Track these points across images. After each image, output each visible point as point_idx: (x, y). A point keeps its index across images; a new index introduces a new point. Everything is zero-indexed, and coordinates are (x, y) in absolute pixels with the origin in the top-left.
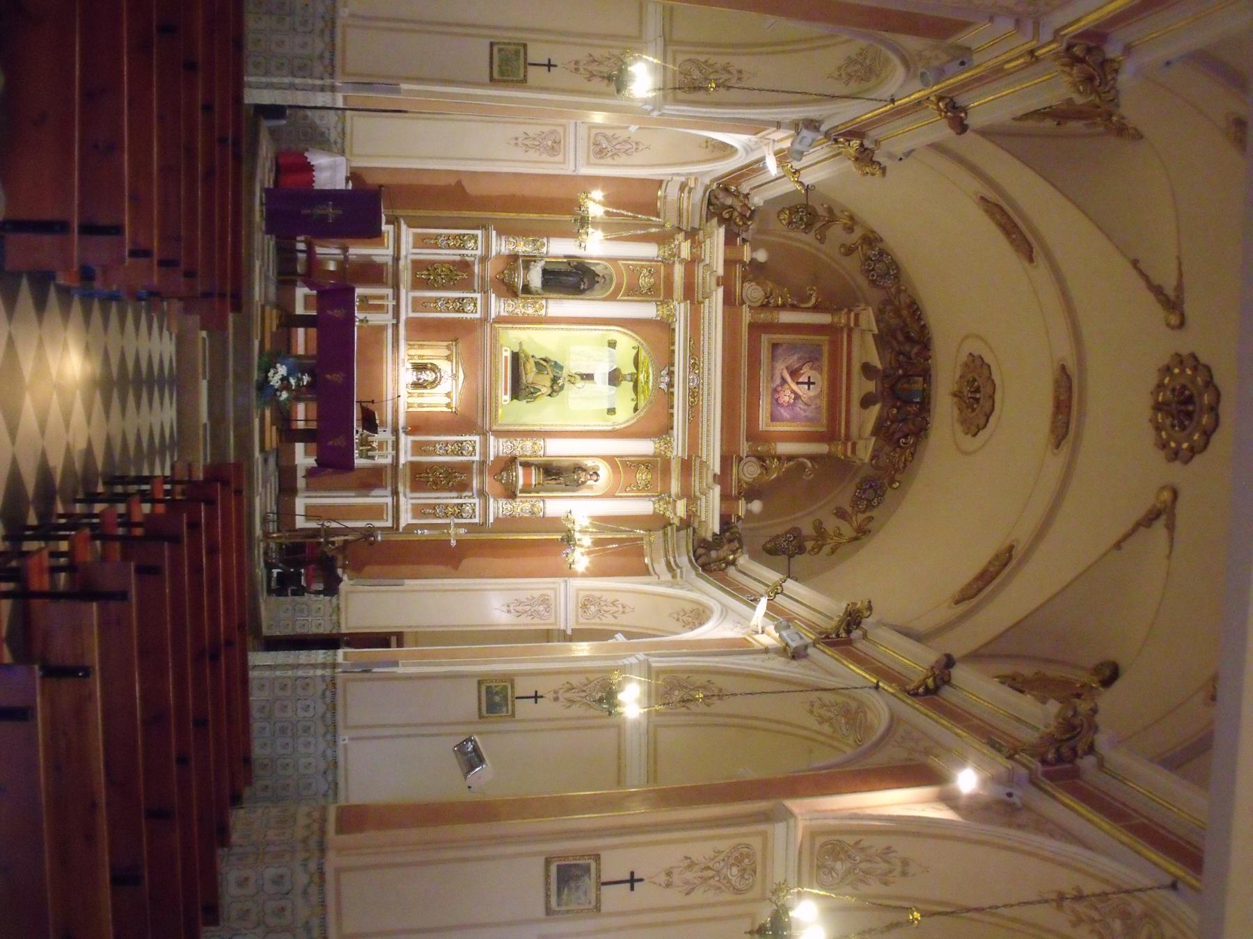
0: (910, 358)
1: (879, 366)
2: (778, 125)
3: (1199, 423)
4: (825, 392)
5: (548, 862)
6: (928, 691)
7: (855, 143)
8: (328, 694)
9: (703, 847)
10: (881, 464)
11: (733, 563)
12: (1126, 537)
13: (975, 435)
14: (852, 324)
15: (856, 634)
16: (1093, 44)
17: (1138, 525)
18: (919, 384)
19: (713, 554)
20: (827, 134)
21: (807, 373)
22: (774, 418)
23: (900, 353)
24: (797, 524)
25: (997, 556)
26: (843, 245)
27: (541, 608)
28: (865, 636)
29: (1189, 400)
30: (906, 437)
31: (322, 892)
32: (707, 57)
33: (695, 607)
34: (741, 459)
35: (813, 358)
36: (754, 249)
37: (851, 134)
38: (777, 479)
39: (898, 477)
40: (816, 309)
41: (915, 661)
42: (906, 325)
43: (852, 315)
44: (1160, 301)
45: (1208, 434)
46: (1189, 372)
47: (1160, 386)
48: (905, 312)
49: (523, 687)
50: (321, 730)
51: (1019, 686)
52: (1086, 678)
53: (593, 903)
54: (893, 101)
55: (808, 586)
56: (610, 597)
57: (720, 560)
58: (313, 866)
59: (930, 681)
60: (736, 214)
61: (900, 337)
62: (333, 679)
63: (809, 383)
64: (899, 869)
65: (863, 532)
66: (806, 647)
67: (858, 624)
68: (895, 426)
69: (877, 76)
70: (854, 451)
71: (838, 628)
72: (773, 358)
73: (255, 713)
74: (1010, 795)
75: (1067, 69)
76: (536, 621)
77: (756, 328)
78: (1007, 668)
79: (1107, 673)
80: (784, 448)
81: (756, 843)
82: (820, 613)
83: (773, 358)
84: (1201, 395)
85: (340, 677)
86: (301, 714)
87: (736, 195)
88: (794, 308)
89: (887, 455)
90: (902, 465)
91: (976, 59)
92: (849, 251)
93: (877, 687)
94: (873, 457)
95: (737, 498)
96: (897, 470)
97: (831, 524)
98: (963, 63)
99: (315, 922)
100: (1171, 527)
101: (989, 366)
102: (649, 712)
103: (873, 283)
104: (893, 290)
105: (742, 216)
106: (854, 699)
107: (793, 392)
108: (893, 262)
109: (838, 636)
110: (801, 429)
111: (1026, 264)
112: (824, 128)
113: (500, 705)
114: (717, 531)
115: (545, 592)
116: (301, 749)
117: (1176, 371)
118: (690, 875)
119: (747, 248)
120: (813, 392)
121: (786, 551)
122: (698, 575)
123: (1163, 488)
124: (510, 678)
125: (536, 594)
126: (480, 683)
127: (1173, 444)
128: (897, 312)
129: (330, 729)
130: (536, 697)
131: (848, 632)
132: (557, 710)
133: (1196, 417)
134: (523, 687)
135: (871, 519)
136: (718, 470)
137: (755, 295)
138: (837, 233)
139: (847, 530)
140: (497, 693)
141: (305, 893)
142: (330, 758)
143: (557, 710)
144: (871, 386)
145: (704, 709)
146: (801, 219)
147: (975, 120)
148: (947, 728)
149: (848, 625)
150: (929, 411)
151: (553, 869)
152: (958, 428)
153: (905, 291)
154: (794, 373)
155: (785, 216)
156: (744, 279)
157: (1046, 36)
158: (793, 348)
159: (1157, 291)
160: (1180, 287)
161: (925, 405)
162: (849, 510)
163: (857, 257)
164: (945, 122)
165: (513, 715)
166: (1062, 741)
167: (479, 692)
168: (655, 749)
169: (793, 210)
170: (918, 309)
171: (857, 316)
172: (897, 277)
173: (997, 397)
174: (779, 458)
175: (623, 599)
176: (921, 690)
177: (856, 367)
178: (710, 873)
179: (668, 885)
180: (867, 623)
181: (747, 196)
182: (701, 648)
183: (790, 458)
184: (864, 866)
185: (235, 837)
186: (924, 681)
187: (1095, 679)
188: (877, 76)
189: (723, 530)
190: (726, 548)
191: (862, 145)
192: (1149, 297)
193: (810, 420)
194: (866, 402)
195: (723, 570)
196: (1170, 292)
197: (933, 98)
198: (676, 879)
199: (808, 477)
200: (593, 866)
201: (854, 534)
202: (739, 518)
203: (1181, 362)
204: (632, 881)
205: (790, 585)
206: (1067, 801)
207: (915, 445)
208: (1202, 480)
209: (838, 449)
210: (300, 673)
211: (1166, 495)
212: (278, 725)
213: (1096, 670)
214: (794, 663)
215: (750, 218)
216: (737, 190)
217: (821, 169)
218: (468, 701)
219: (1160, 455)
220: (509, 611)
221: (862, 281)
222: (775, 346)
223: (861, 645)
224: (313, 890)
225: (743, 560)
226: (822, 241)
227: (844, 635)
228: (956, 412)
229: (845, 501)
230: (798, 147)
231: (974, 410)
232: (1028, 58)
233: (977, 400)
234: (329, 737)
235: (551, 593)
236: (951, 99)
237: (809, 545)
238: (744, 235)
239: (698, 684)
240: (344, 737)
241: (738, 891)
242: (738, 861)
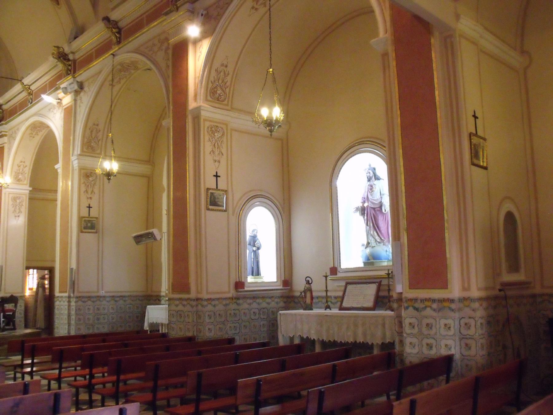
5: (208, 209)
8: (83, 300)
9: (207, 146)
15: (71, 57)
27: (18, 201)
28: (73, 53)
31: (214, 300)
33: (30, 128)
41: (96, 34)
49: (85, 213)
50: (98, 303)
53: (223, 192)
56: (16, 168)
58: (205, 303)
62: (77, 297)
64: (224, 68)
67: (66, 55)
71: (64, 64)
73: (91, 332)
74: (202, 15)
76: (24, 204)
81: (207, 124)
82: (50, 70)
85: (76, 294)
86: (91, 312)
99: (224, 302)
102: (115, 157)
109: (70, 65)
113: (92, 224)
115: (10, 199)
116: (106, 311)
118: (217, 153)
122: (6, 124)
124: (80, 218)
125: (11, 203)
126: (82, 232)
129: (446, 304)
130: (89, 207)
131: (69, 60)
132: (95, 197)
134: (85, 213)
140: (87, 224)
141: (214, 306)
142: (461, 305)
143: (95, 197)
145: (101, 133)
148: (148, 30)
149: (65, 59)
151: (211, 207)
165: (97, 218)
167: (86, 232)
168: (139, 160)
175: (17, 162)
178: (216, 144)
179: (219, 162)
180: (67, 50)
184: (220, 82)
185: (190, 334)
195: (3, 111)
198: (217, 159)
200: (211, 191)
204: (217, 176)
205: (26, 81)
210: (73, 312)
212: (96, 322)
214: (86, 89)
218: (89, 237)
220: (19, 216)
224: (213, 303)
227: (70, 63)
234: (101, 299)
235: (11, 196)
240: (102, 293)
241: (223, 135)
242: (213, 132)
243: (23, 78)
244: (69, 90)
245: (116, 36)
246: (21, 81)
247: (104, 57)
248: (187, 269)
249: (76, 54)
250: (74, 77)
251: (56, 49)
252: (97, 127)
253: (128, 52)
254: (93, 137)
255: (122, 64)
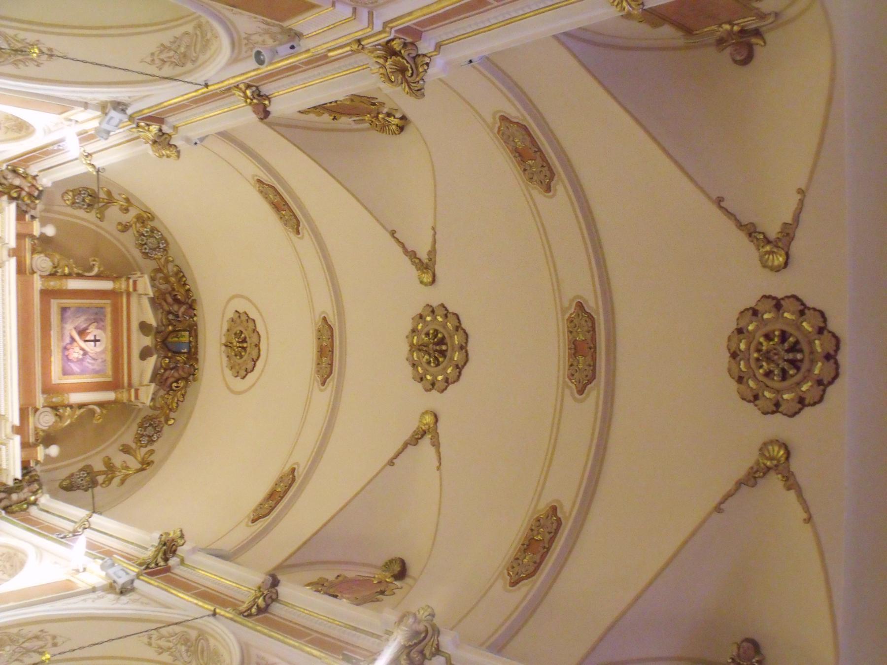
0: (177, 316)
1: (154, 324)
2: (86, 105)
3: (452, 359)
4: (110, 347)
6: (260, 611)
7: (154, 128)
10: (158, 405)
11: (35, 503)
12: (397, 456)
13: (244, 378)
14: (131, 289)
15: (173, 561)
16: (409, 40)
17: (406, 445)
18: (185, 337)
19: (14, 497)
20: (131, 118)
21: (93, 332)
22: (65, 372)
23: (169, 312)
24: (89, 462)
25: (281, 479)
26: (120, 224)
28: (182, 562)
29: (442, 341)
30: (177, 381)
32: (16, 32)
34: (36, 410)
35: (97, 318)
36: (43, 224)
37: (157, 119)
38: (70, 425)
39: (172, 415)
40: (98, 277)
41: (242, 580)
42: (174, 289)
43: (131, 281)
44: (413, 263)
45: (459, 368)
46: (439, 319)
47: (414, 331)
48: (173, 279)
51: (331, 591)
52: (379, 574)
54: (207, 85)
55: (113, 518)
57: (20, 502)
59: (260, 601)
60: (24, 193)
61: (170, 300)
63: (96, 341)
65: (146, 464)
66: (132, 581)
67: (174, 552)
68: (167, 373)
69: (194, 61)
70: (137, 397)
71: (155, 557)
72: (63, 319)
75: (381, 61)
77: (47, 294)
78: (314, 575)
79: (397, 568)
80: (76, 398)
83: (63, 319)
84: (452, 337)
87: (25, 177)
88: (80, 276)
89: (162, 397)
90: (175, 405)
91: (305, 44)
92: (125, 228)
93: (214, 614)
94: (153, 399)
95: (35, 445)
96: (171, 410)
97: (119, 459)
98: (292, 47)
100: (436, 444)
101: (254, 321)
103: (146, 255)
104: (163, 260)
105: (30, 195)
106: (193, 628)
107: (82, 349)
108: (163, 238)
109: (157, 564)
110: (89, 380)
111: (293, 236)
112: (130, 111)
114: (19, 476)
117: (429, 319)
119: (36, 224)
120: (100, 347)
121: (80, 485)
123: (426, 412)
127: (429, 377)
128: (166, 279)
131: (166, 560)
133: (448, 354)
135: (152, 452)
136: (17, 422)
137: (44, 266)
138: (114, 213)
139: (134, 464)
144: (148, 341)
146: (84, 200)
147: (277, 108)
149: (165, 553)
150: (197, 360)
152: (228, 373)
153: (172, 261)
154: (82, 333)
155: (69, 196)
156: (34, 251)
157: (378, 27)
158: (80, 310)
159: (412, 255)
160: (433, 252)
161: (193, 355)
162: (133, 446)
163: (131, 233)
164: (249, 109)
166: (410, 646)
169: (77, 192)
170: (184, 276)
171: (135, 282)
172: (165, 250)
173: (263, 346)
174: (71, 406)
176: (254, 610)
177: (135, 326)
180: (181, 551)
181: (34, 177)
182: (27, 598)
183: (81, 406)
186: (254, 602)
187: (388, 574)
188: (194, 61)
189: (24, 475)
190: (26, 490)
191: (160, 130)
192: (406, 260)
193: (96, 372)
194: (145, 354)
196: (423, 255)
197: (242, 86)
199: (97, 421)
201: (139, 466)
202: (37, 462)
203: (433, 312)
206: (292, 642)
207: (185, 387)
208: (824, 435)
209: (124, 396)
211: (429, 419)
213: (388, 565)
214: (124, 599)
215: (38, 198)
216: (24, 173)
217: (116, 154)
219: (419, 386)
221: (137, 254)
222: (64, 310)
223: (180, 571)
225: (44, 499)
226: (101, 219)
227: (162, 563)
228: (225, 359)
229: (128, 438)
230: (105, 126)
231: (241, 357)
232: (355, 47)
233: (244, 349)
236: (257, 88)
237: (100, 479)
238: (33, 212)
239: (30, 635)
243: (101, 514)
244: (111, 571)
245: (252, 607)
246: (94, 512)
247: (200, 603)
248: (42, 343)
249: (182, 567)
250: (138, 576)
251: (178, 533)
252: (50, 645)
253: (234, 634)
254: (26, 645)
255: (202, 635)
